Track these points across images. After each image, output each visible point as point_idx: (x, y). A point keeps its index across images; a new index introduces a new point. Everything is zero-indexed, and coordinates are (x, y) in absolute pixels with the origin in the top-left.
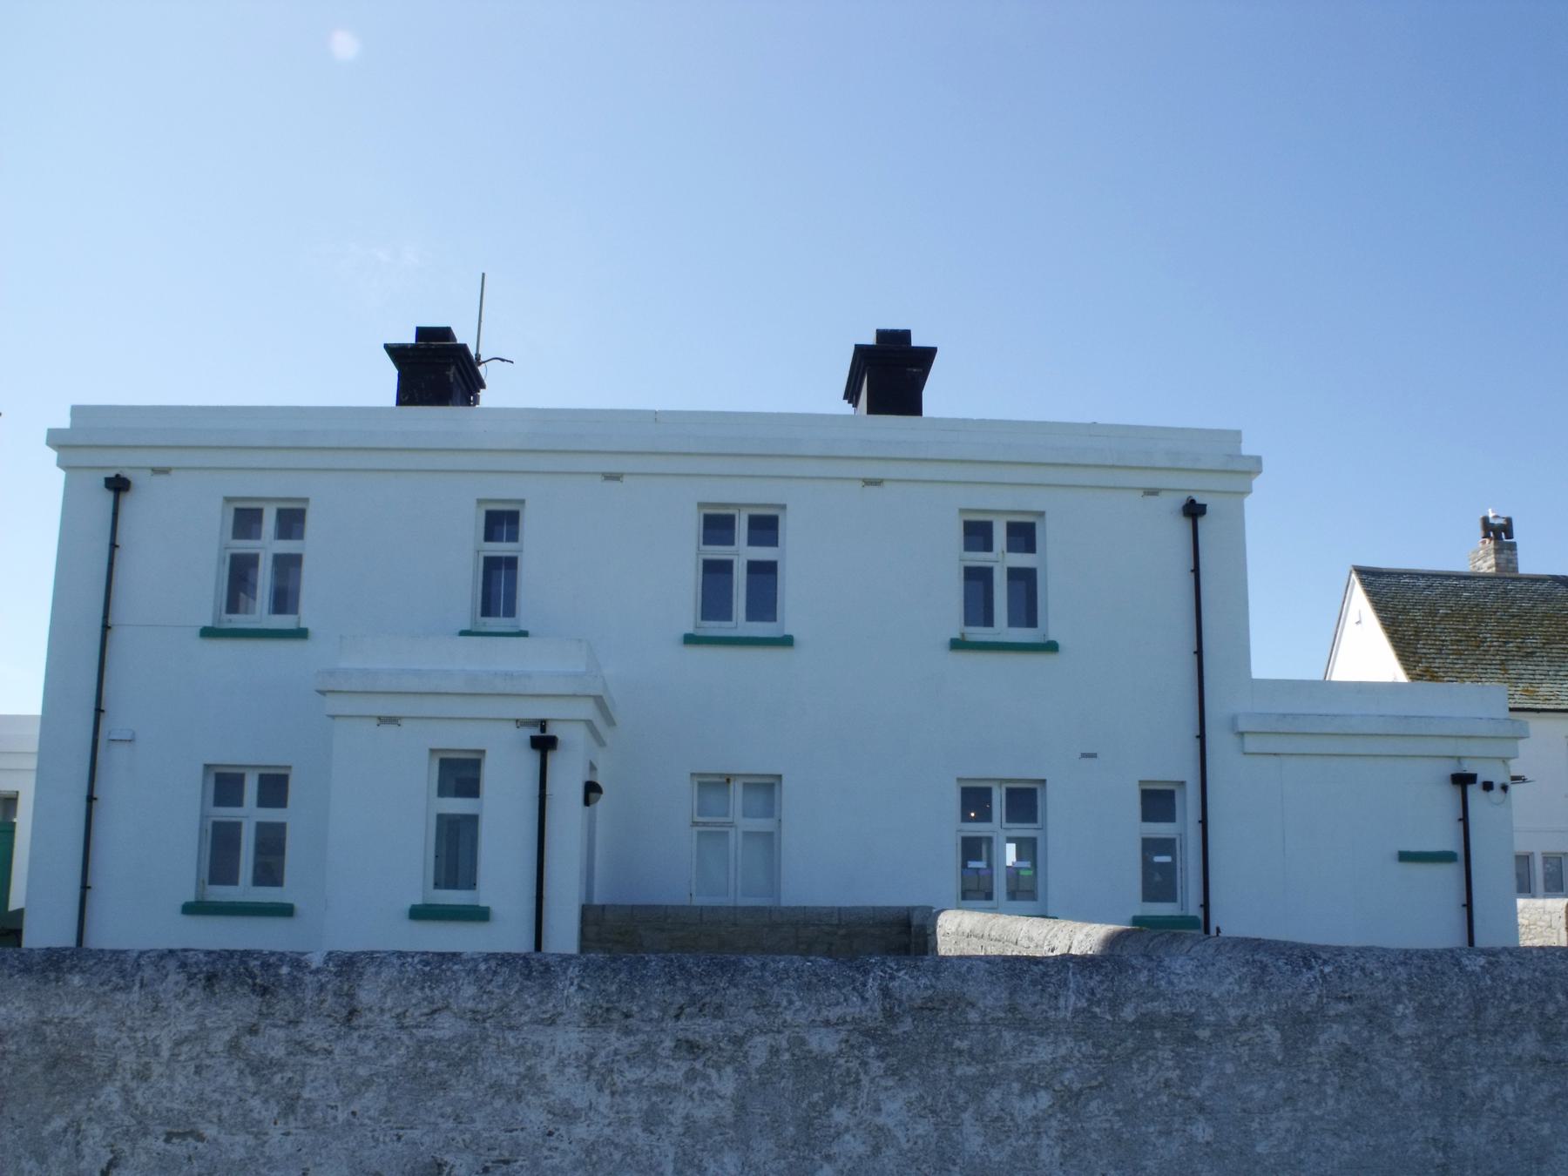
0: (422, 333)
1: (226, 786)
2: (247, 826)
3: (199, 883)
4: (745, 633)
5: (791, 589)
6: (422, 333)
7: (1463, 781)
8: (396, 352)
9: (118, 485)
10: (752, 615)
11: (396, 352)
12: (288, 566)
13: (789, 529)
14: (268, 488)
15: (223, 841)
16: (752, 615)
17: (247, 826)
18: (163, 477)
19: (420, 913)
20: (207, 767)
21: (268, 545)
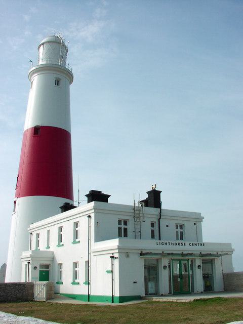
7: (112, 257)
11: (86, 196)
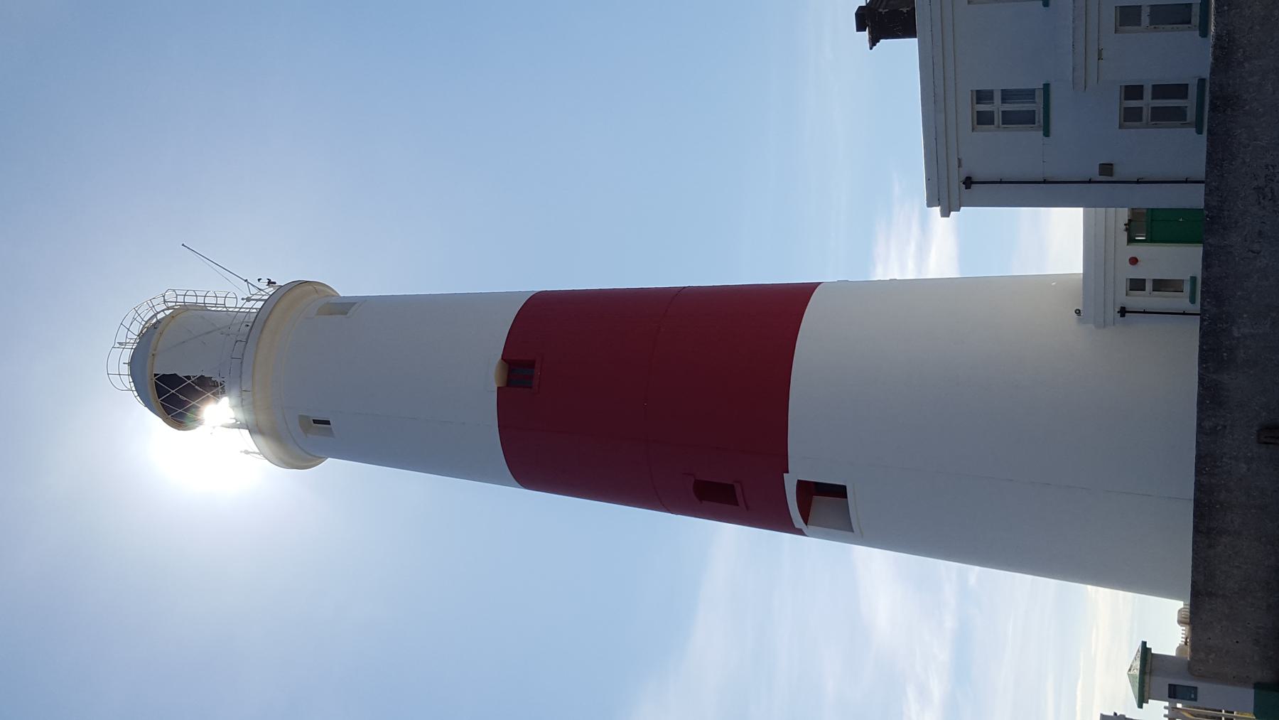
0: (860, 27)
1: (1131, 117)
2: (1147, 105)
3: (1184, 125)
4: (1195, 101)
5: (1169, 77)
6: (860, 27)
8: (873, 42)
9: (968, 182)
10: (1185, 96)
11: (873, 42)
12: (1007, 96)
13: (1133, 80)
14: (966, 112)
15: (1161, 116)
16: (1185, 96)
17: (1147, 105)
18: (963, 162)
19: (1204, 33)
20: (1120, 127)
21: (997, 107)
